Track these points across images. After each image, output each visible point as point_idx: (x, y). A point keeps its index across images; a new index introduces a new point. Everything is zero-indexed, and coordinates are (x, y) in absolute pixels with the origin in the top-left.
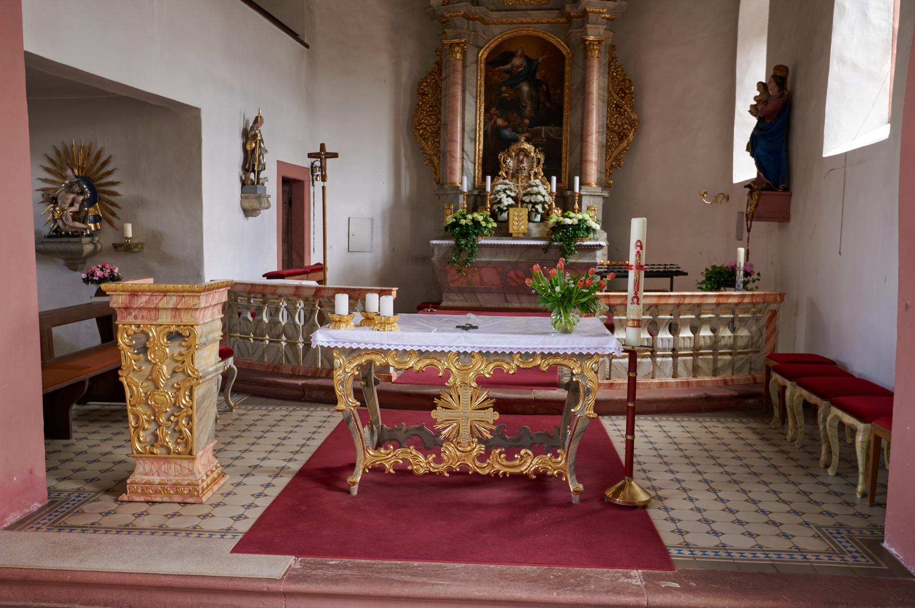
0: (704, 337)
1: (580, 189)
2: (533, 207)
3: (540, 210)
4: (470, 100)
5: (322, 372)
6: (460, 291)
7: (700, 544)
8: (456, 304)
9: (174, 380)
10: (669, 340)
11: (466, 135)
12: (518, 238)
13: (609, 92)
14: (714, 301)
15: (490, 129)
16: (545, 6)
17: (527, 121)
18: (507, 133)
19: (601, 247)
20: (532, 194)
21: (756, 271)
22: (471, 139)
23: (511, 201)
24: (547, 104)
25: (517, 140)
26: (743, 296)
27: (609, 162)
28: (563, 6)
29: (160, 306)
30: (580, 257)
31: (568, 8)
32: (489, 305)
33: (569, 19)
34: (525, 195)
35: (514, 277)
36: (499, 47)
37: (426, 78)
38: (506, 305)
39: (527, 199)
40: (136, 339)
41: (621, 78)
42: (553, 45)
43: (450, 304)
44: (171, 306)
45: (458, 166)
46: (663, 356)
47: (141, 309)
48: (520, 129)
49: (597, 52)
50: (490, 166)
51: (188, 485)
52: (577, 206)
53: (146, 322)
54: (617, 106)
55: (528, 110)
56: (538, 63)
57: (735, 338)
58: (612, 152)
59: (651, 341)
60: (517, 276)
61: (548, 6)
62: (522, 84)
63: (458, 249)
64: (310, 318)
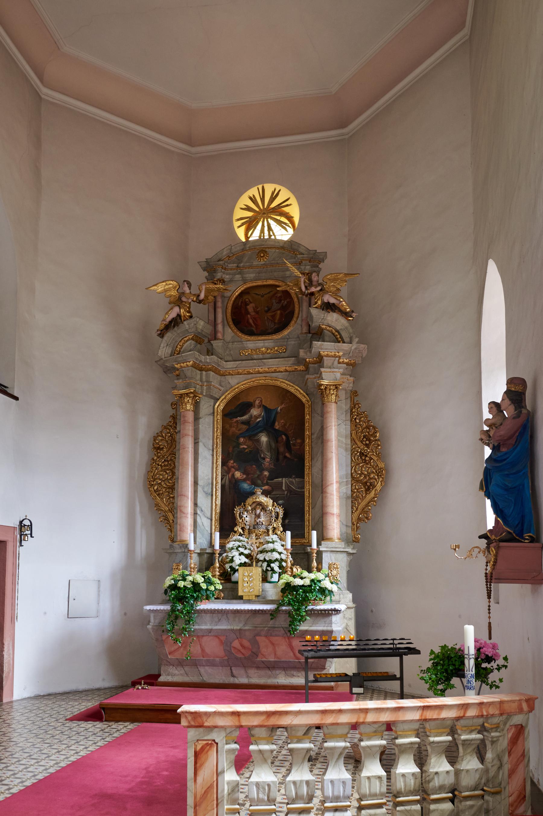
0: (403, 775)
1: (319, 544)
2: (269, 565)
3: (276, 569)
4: (205, 453)
6: (180, 663)
8: (176, 679)
11: (200, 489)
12: (249, 601)
13: (353, 440)
14: (416, 716)
17: (266, 473)
18: (246, 486)
19: (337, 611)
20: (267, 552)
21: (502, 652)
23: (244, 559)
24: (288, 455)
25: (253, 493)
26: (465, 707)
27: (356, 515)
28: (298, 353)
30: (313, 624)
31: (302, 353)
32: (212, 681)
33: (307, 365)
34: (261, 552)
35: (240, 648)
36: (235, 398)
37: (161, 432)
38: (232, 680)
39: (261, 557)
42: (292, 394)
43: (170, 679)
45: (188, 522)
48: (259, 482)
49: (334, 397)
50: (227, 524)
52: (315, 564)
54: (362, 454)
55: (267, 462)
56: (277, 413)
57: (457, 773)
61: (286, 355)
62: (261, 434)
63: (173, 616)
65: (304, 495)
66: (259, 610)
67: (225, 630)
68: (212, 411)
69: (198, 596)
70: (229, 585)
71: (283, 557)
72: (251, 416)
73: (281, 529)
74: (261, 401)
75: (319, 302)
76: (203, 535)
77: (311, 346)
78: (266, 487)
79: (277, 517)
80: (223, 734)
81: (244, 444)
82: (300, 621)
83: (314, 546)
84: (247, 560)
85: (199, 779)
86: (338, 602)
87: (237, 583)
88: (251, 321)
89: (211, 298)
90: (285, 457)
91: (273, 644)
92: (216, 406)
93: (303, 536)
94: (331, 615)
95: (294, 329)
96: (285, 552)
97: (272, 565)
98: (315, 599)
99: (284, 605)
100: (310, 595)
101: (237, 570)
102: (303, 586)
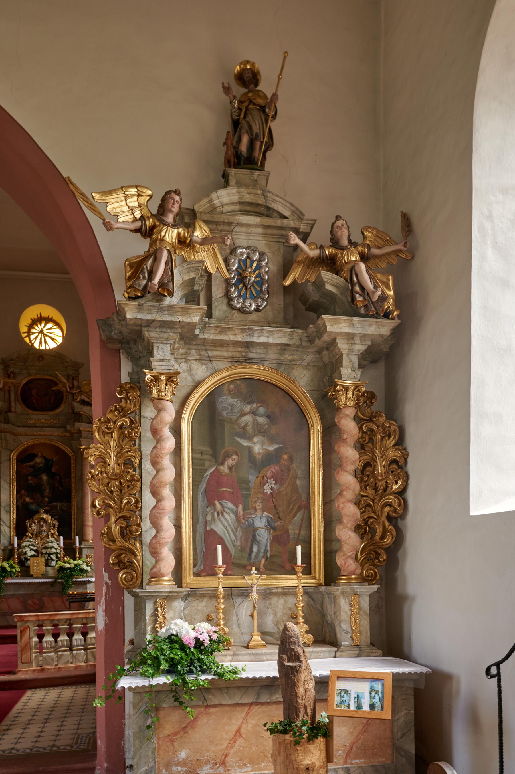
1: (80, 543)
2: (49, 556)
10: (81, 640)
12: (37, 578)
15: (20, 505)
17: (47, 499)
18: (33, 507)
19: (90, 582)
20: (48, 548)
22: (6, 511)
23: (33, 553)
24: (60, 488)
25: (38, 512)
31: (68, 427)
33: (72, 434)
36: (25, 450)
39: (44, 551)
42: (62, 450)
46: (78, 650)
48: (42, 504)
50: (21, 531)
52: (78, 555)
59: (68, 641)
60: (34, 603)
62: (42, 475)
65: (71, 513)
66: (44, 582)
67: (23, 594)
68: (9, 458)
69: (5, 575)
70: (24, 568)
71: (58, 551)
72: (36, 463)
73: (57, 534)
74: (42, 454)
75: (79, 399)
76: (5, 537)
77: (74, 424)
78: (46, 508)
80: (32, 623)
81: (31, 481)
82: (68, 588)
83: (77, 544)
84: (35, 553)
85: (23, 641)
86: (92, 577)
87: (29, 567)
88: (34, 401)
89: (7, 388)
91: (52, 601)
92: (12, 455)
93: (71, 538)
94: (87, 583)
96: (59, 548)
97: (51, 556)
98: (77, 575)
99: (59, 579)
100: (74, 573)
101: (29, 559)
102: (70, 568)
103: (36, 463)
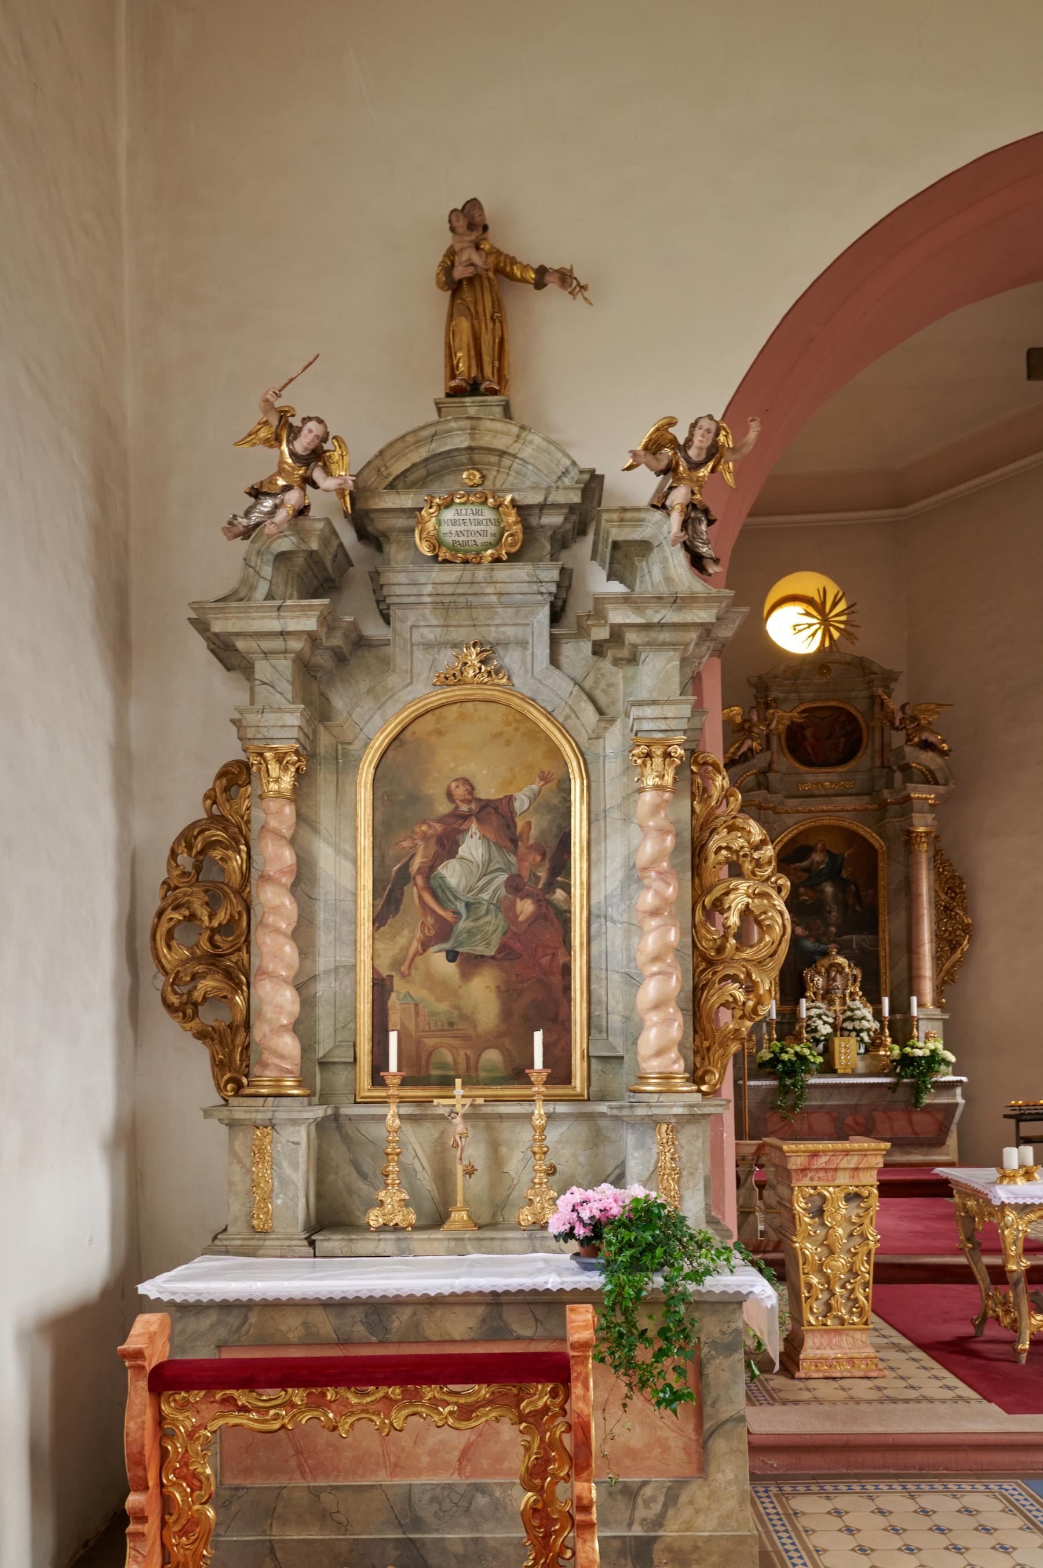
3: (866, 1039)
5: (767, 1245)
7: (940, 1498)
9: (851, 1244)
13: (936, 891)
16: (850, 791)
17: (833, 929)
18: (809, 944)
24: (858, 908)
29: (842, 1166)
30: (936, 1096)
33: (883, 806)
39: (849, 1025)
40: (812, 1202)
41: (949, 875)
44: (852, 1166)
47: (817, 1170)
51: (866, 1358)
53: (822, 1183)
54: (946, 908)
56: (843, 859)
58: (943, 965)
62: (825, 884)
64: (746, 1180)
67: (839, 1105)
72: (812, 862)
75: (916, 740)
79: (855, 981)
88: (809, 749)
90: (856, 910)
91: (890, 1119)
95: (863, 761)
103: (812, 862)
